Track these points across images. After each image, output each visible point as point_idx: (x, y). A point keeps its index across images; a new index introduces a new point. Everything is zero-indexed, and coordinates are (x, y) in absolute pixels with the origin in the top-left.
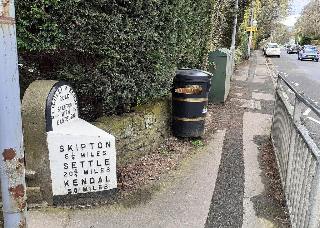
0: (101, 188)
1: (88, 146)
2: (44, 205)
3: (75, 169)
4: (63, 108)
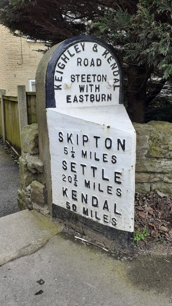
0: (107, 221)
1: (92, 141)
2: (45, 211)
3: (75, 174)
4: (82, 78)
